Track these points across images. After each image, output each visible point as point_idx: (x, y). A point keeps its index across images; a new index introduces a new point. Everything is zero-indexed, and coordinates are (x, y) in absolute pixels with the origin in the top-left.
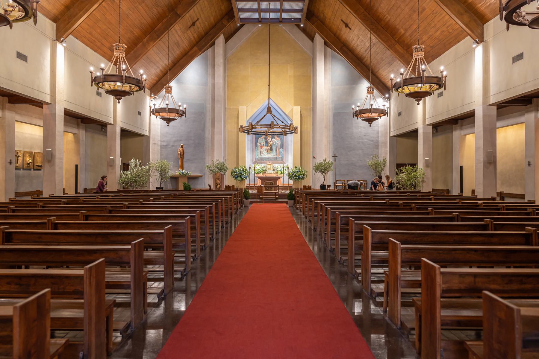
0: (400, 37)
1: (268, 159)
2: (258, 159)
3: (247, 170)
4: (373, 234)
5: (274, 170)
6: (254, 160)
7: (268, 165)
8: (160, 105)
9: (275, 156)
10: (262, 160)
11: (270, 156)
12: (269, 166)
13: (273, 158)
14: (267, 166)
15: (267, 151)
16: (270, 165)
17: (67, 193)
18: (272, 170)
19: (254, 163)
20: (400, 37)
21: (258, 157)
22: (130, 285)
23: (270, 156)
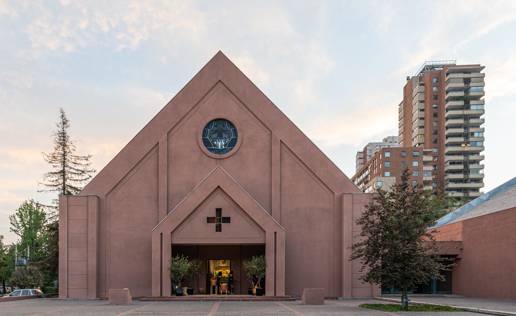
0: (56, 226)
1: (223, 267)
2: (217, 267)
3: (211, 274)
4: (482, 145)
5: (226, 273)
6: (215, 268)
7: (223, 270)
8: (431, 176)
9: (227, 265)
10: (219, 268)
11: (224, 265)
12: (224, 271)
13: (226, 266)
14: (223, 271)
15: (223, 263)
16: (224, 270)
17: (223, 228)
18: (225, 273)
19: (215, 269)
20: (56, 226)
21: (217, 266)
22: (226, 294)
23: (224, 265)
